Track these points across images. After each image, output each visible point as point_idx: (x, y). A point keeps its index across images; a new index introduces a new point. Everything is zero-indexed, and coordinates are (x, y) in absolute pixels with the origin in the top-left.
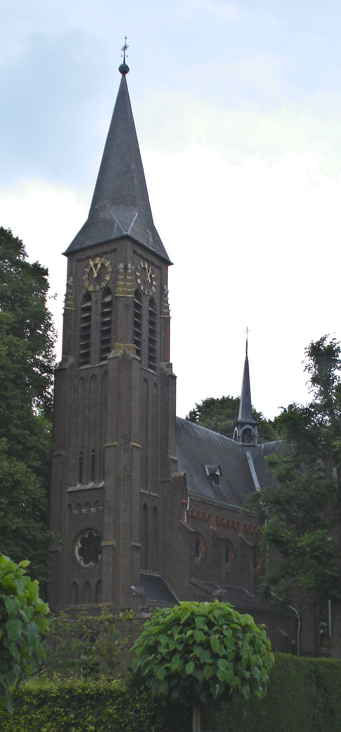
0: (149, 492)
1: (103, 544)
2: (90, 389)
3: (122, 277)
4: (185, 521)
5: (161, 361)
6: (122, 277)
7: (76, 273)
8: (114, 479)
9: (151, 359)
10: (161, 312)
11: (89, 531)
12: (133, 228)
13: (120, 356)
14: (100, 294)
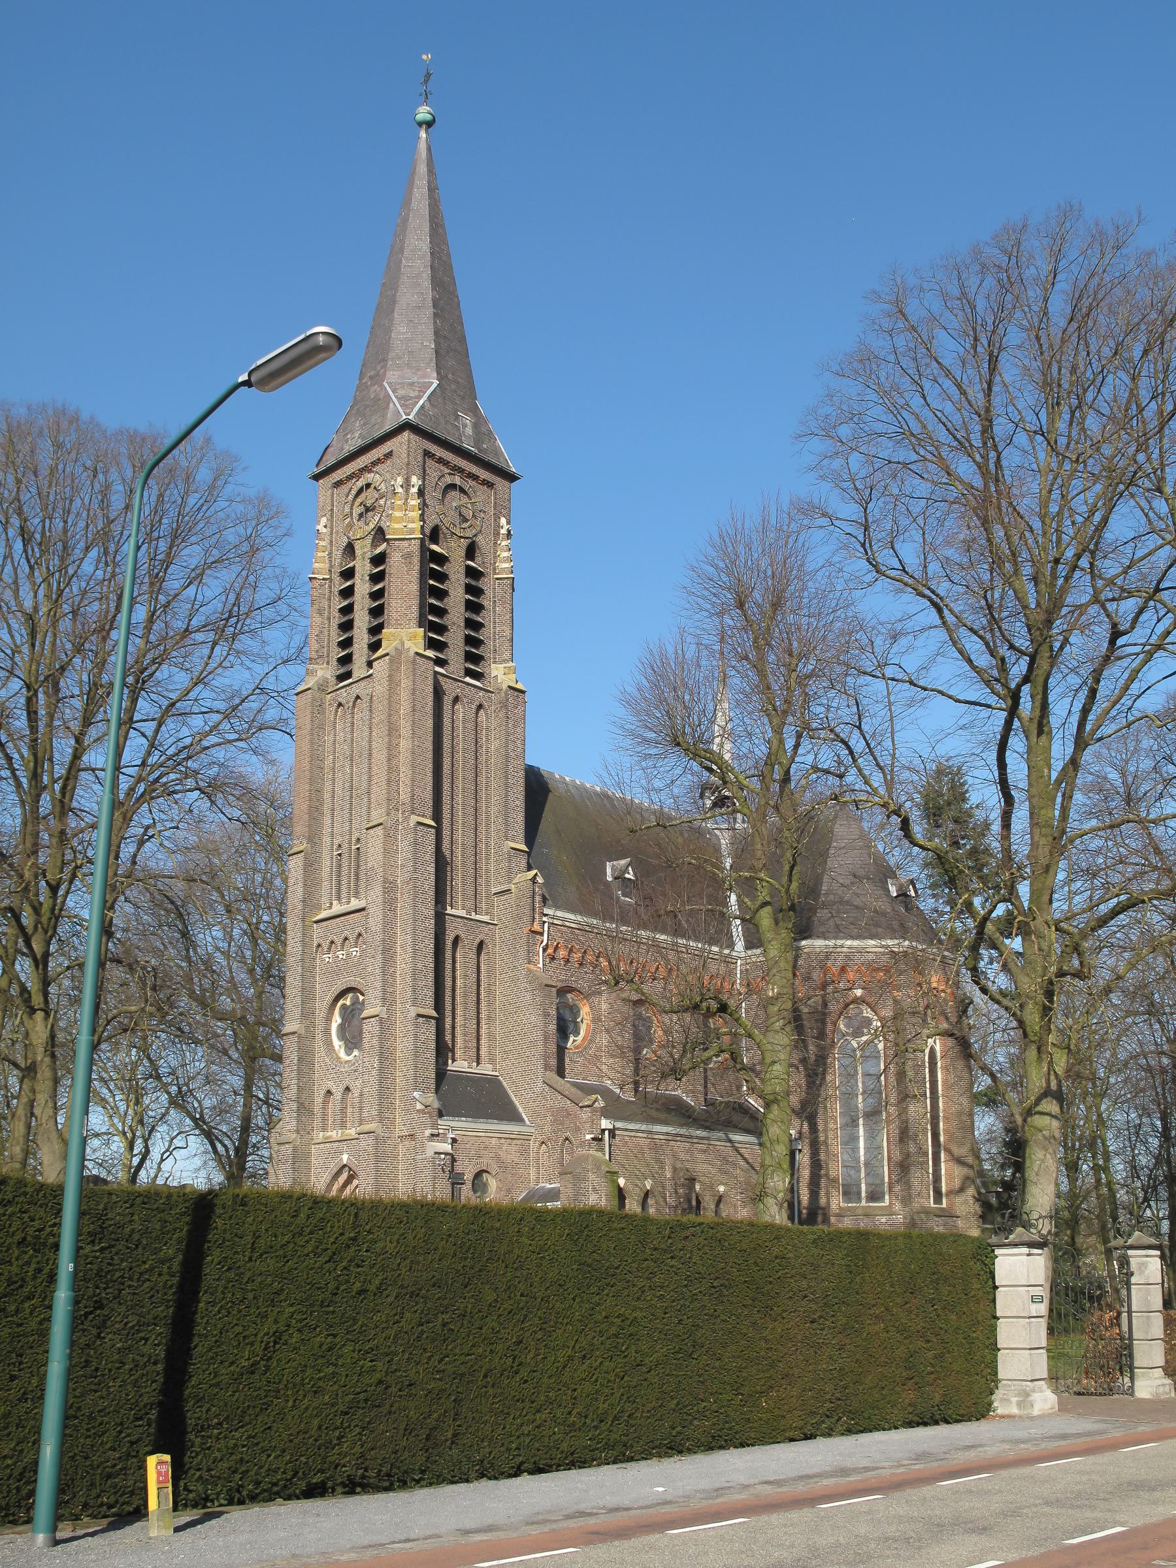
0: (469, 913)
1: (365, 1014)
2: (353, 723)
3: (399, 502)
4: (541, 965)
5: (495, 662)
6: (399, 502)
7: (332, 510)
8: (135, 818)
9: (472, 658)
10: (495, 569)
11: (351, 995)
12: (422, 407)
13: (393, 653)
14: (369, 540)
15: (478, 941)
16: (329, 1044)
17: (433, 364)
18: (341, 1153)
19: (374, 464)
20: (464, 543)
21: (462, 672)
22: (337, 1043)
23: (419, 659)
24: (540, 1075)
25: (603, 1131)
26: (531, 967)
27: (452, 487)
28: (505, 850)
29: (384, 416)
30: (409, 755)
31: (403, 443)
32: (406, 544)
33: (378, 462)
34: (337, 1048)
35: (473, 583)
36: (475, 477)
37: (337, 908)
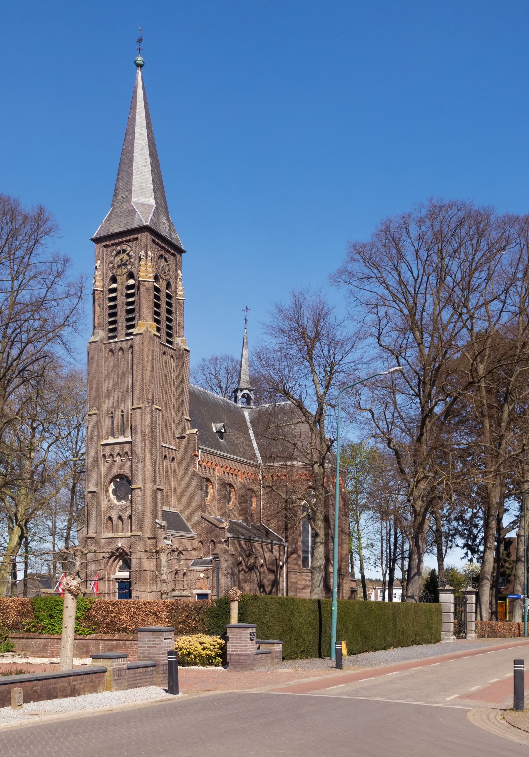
0: (169, 445)
15: (172, 457)
16: (108, 497)
17: (153, 196)
18: (118, 543)
19: (127, 241)
20: (165, 282)
21: (166, 341)
22: (112, 496)
23: (155, 337)
24: (199, 514)
25: (228, 538)
26: (194, 469)
27: (161, 256)
28: (183, 419)
29: (133, 219)
30: (490, 526)
31: (145, 238)
32: (147, 283)
33: (129, 241)
34: (112, 498)
35: (169, 301)
36: (169, 252)
37: (111, 440)
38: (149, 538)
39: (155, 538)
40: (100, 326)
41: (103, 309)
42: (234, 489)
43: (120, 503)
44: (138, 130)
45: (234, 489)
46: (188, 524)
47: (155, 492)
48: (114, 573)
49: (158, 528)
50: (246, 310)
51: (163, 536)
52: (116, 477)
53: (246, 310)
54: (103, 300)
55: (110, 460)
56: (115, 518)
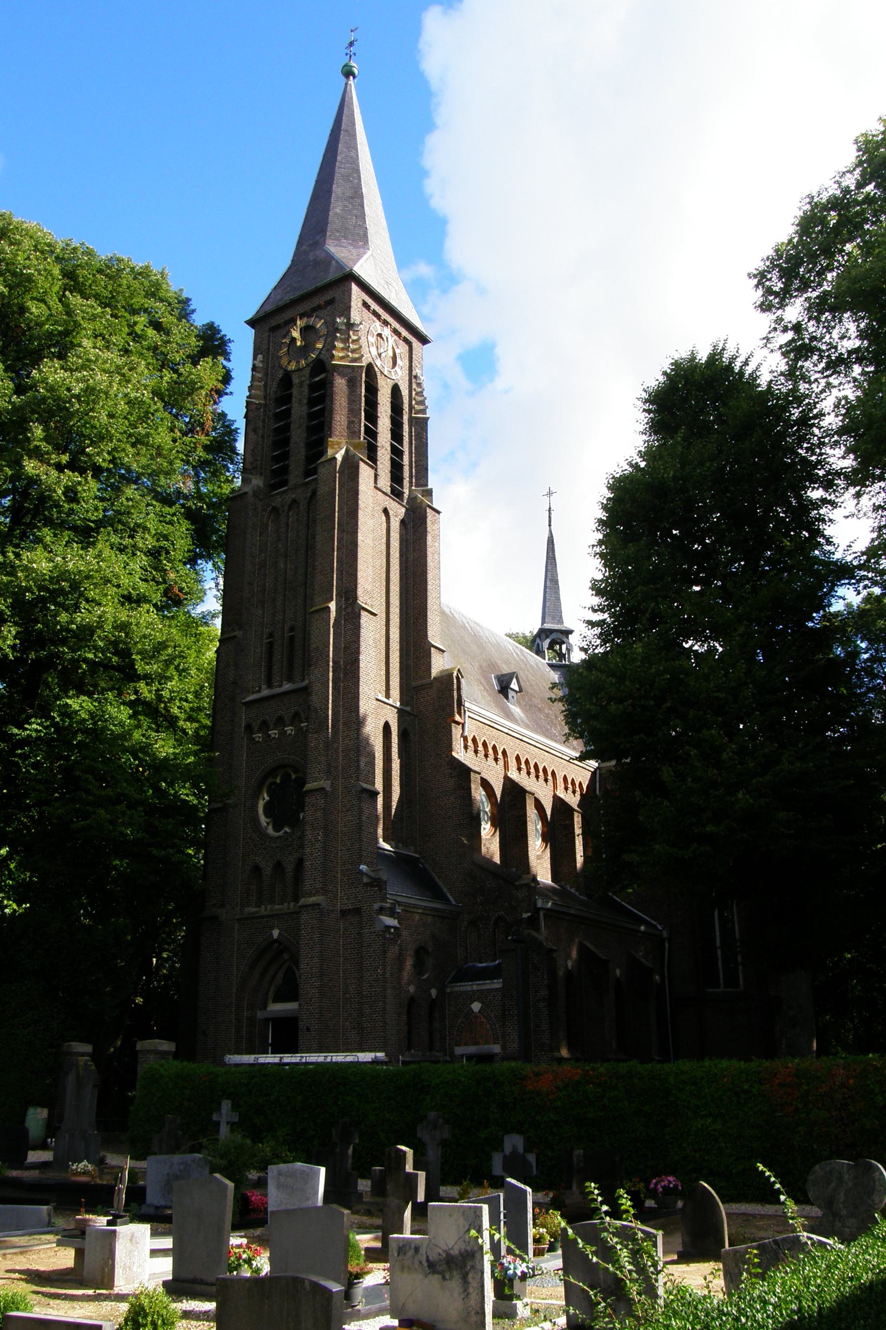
16: (256, 820)
19: (314, 310)
22: (263, 819)
33: (319, 308)
38: (344, 913)
39: (357, 911)
40: (255, 468)
41: (263, 437)
42: (576, 759)
43: (281, 833)
44: (381, 753)
45: (576, 759)
46: (441, 884)
47: (359, 798)
48: (265, 1007)
49: (366, 884)
50: (550, 494)
51: (376, 906)
52: (272, 772)
53: (550, 494)
54: (264, 421)
55: (258, 736)
56: (267, 869)
